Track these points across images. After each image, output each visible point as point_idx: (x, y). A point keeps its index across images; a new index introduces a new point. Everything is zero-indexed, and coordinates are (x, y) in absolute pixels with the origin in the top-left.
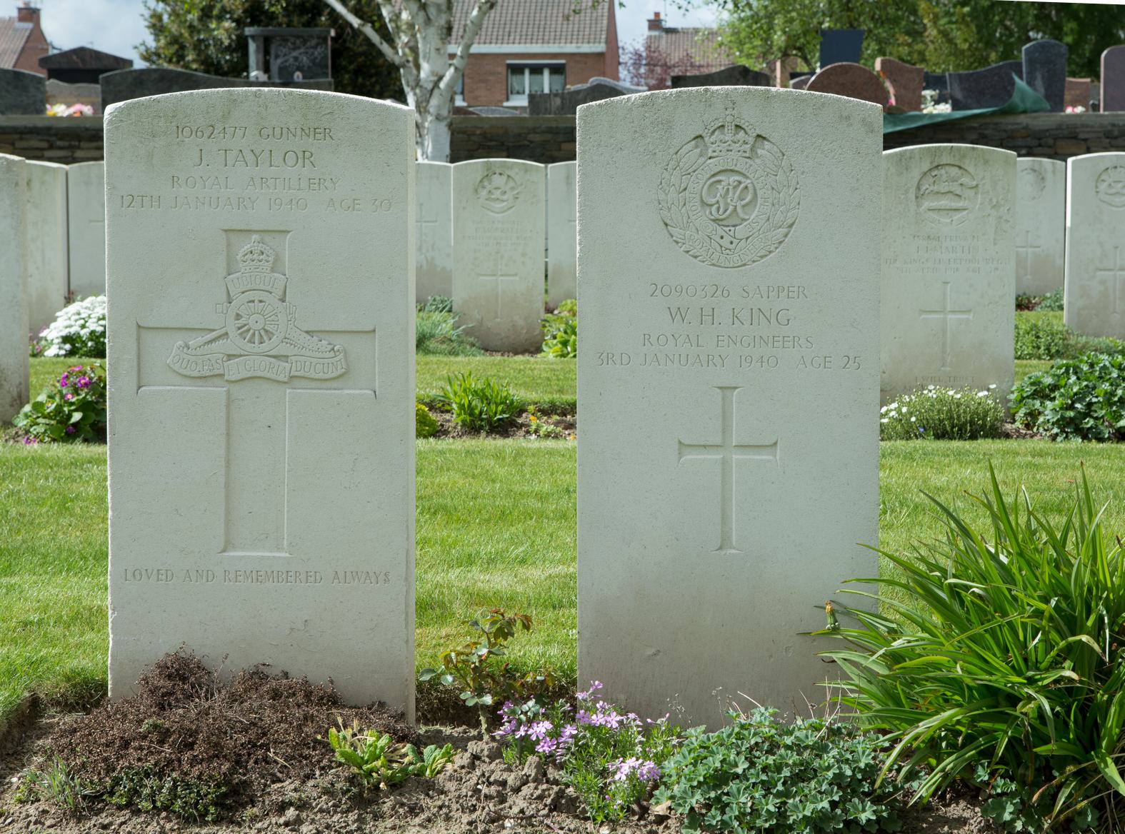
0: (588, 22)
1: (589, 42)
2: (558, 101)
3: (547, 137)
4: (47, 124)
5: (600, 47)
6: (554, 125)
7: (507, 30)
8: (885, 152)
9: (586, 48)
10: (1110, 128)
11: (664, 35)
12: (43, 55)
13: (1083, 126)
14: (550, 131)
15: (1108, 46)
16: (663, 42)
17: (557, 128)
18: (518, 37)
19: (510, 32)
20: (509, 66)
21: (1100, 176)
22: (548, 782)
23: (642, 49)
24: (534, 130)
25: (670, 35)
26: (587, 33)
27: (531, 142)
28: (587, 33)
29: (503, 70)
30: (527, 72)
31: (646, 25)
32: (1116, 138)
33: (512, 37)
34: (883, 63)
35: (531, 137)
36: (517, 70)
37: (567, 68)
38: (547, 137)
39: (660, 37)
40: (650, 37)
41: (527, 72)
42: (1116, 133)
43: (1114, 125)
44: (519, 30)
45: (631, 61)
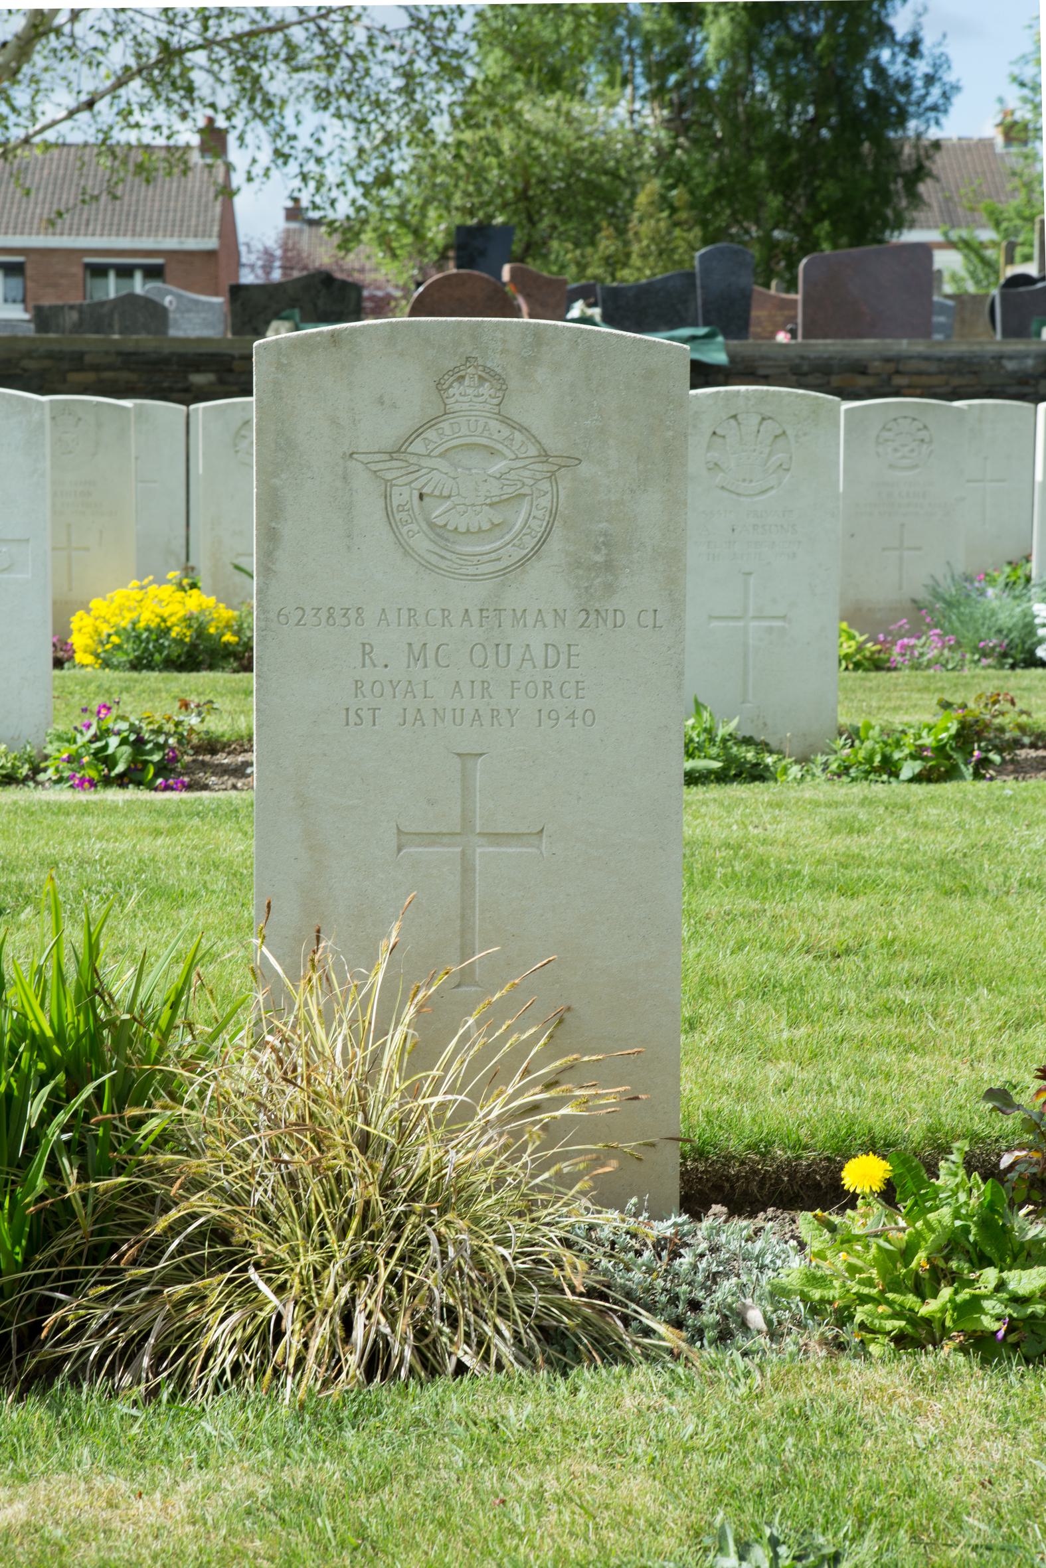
0: (195, 208)
1: (196, 236)
2: (75, 316)
3: (47, 363)
4: (167, 349)
5: (211, 243)
6: (56, 347)
7: (85, 217)
8: (693, 392)
9: (192, 244)
10: (797, 361)
11: (306, 228)
12: (233, 282)
13: (763, 358)
14: (50, 355)
15: (805, 255)
16: (305, 236)
17: (60, 352)
18: (99, 228)
19: (88, 221)
20: (88, 266)
21: (238, 432)
22: (783, 991)
23: (275, 246)
24: (29, 355)
25: (314, 229)
26: (193, 222)
27: (25, 370)
28: (193, 222)
29: (78, 270)
30: (112, 276)
31: (282, 214)
32: (805, 374)
33: (91, 228)
34: (513, 273)
35: (26, 363)
36: (99, 271)
37: (167, 271)
38: (47, 363)
39: (301, 231)
40: (287, 231)
41: (112, 276)
42: (805, 368)
43: (802, 358)
44: (100, 217)
45: (260, 263)
